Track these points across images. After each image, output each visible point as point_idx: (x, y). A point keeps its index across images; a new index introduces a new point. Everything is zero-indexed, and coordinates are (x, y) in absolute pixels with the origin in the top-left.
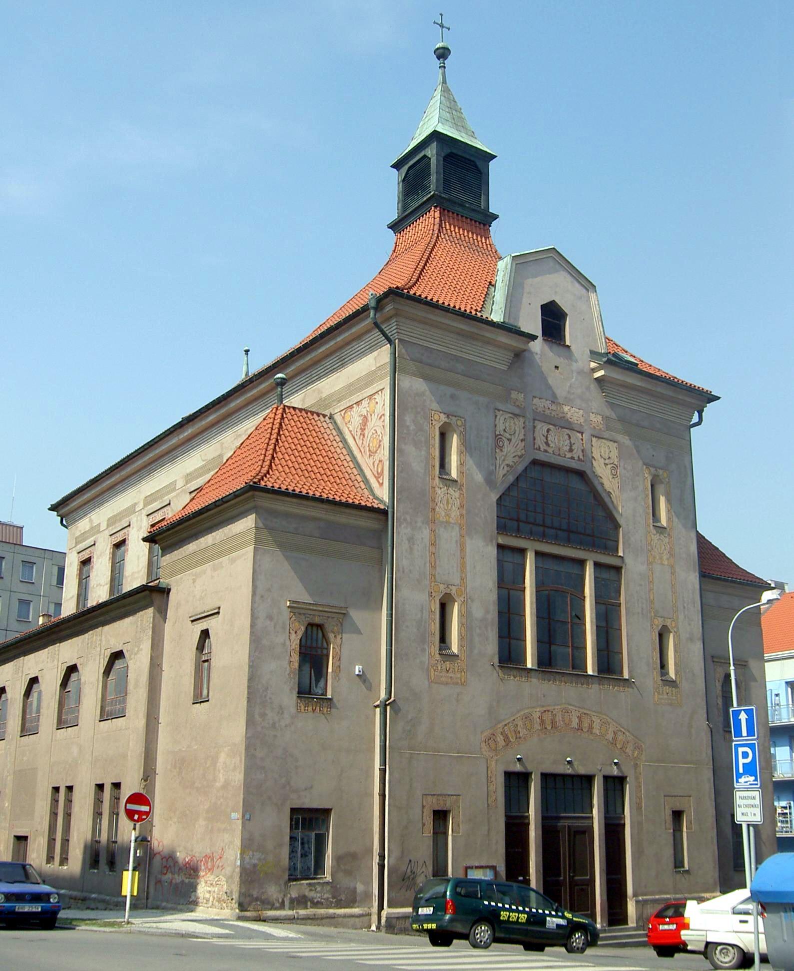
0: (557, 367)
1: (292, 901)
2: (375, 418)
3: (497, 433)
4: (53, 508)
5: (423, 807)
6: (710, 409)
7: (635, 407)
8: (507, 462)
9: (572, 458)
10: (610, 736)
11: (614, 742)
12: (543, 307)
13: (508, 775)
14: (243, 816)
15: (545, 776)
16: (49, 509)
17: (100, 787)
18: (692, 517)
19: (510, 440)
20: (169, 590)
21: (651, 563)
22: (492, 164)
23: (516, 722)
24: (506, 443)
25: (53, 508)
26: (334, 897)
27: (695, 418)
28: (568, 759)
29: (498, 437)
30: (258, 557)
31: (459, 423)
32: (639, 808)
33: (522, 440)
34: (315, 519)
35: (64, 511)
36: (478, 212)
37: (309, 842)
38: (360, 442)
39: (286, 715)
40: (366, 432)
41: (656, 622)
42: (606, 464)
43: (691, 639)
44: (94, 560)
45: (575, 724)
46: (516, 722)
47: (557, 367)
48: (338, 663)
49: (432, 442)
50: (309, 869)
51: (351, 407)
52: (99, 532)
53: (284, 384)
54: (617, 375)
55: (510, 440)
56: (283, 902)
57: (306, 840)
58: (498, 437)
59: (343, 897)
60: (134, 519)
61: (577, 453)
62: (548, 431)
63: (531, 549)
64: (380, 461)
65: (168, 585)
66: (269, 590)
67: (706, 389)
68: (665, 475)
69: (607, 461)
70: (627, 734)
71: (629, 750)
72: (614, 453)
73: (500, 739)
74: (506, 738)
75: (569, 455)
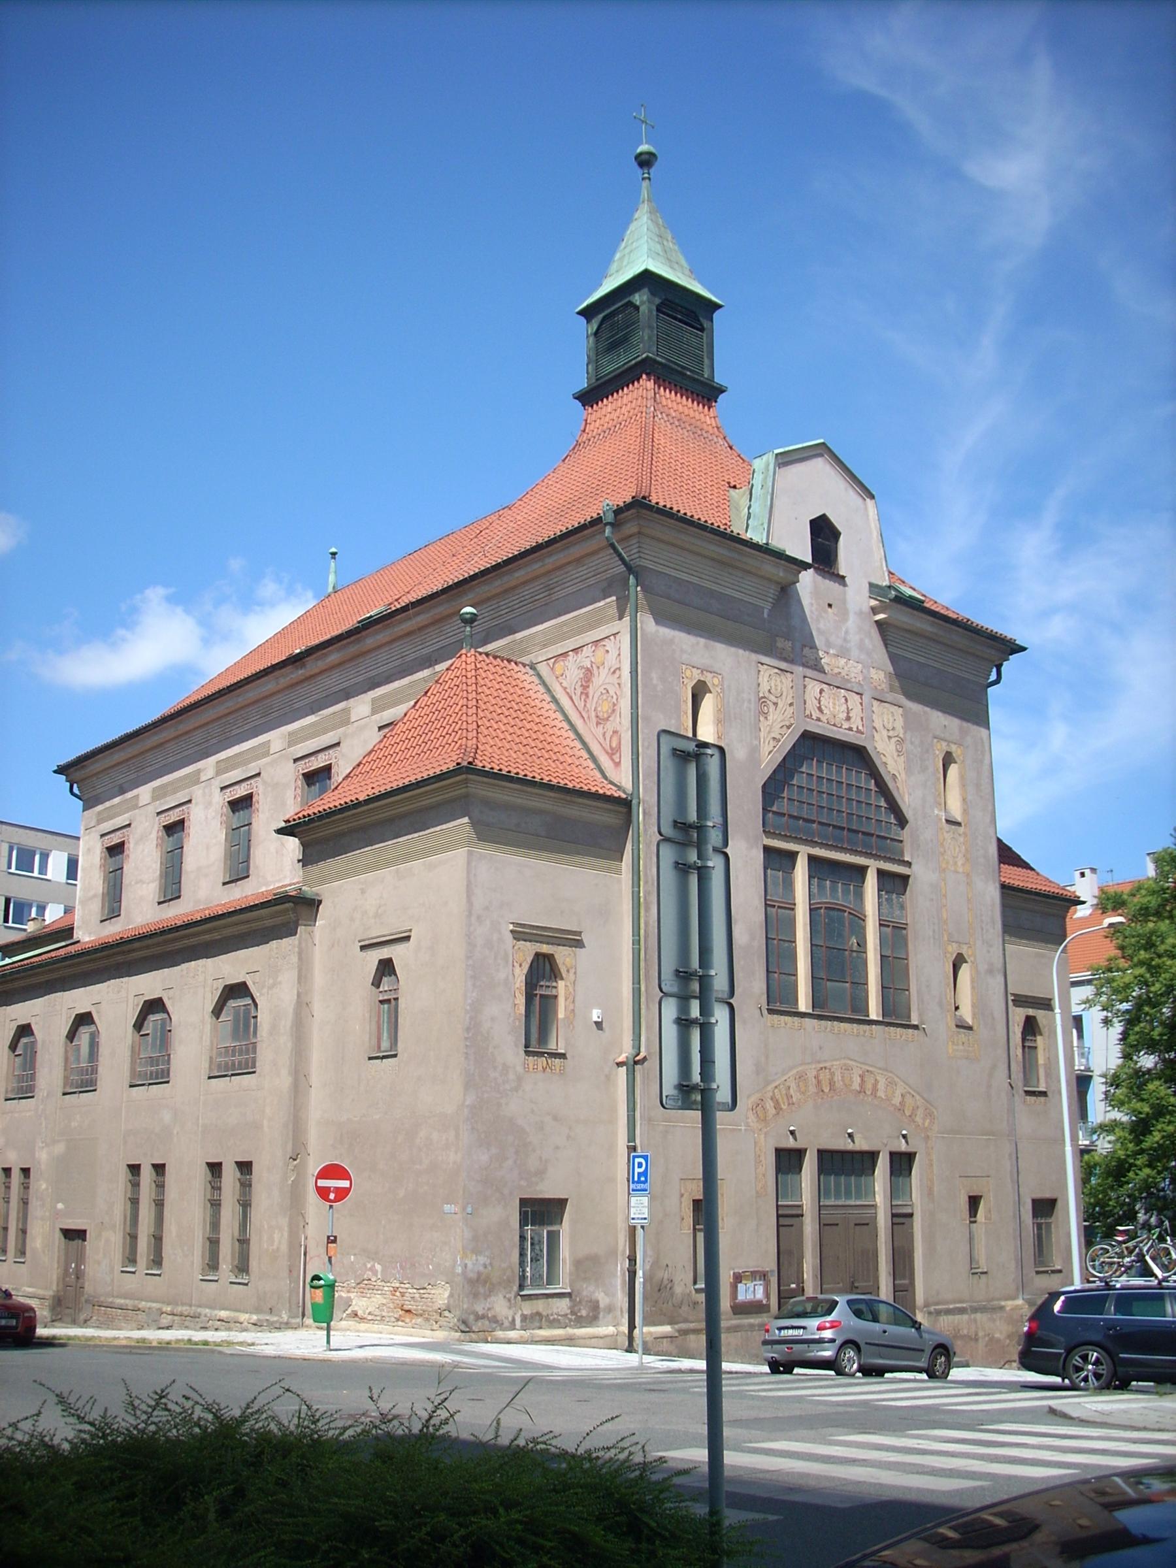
0: (830, 606)
1: (524, 1318)
2: (604, 672)
3: (761, 695)
4: (61, 770)
5: (682, 1195)
6: (1010, 666)
7: (922, 660)
8: (773, 735)
9: (850, 729)
10: (897, 1100)
11: (901, 1109)
12: (812, 522)
13: (779, 1152)
14: (464, 1209)
15: (821, 1153)
16: (55, 772)
17: (215, 1168)
18: (990, 808)
19: (776, 704)
20: (320, 902)
21: (944, 870)
22: (717, 315)
23: (787, 1084)
24: (772, 707)
25: (61, 770)
26: (573, 1313)
27: (993, 677)
28: (850, 1131)
29: (762, 701)
30: (473, 864)
31: (716, 681)
32: (930, 1193)
33: (791, 704)
34: (540, 812)
35: (78, 775)
36: (702, 383)
37: (540, 1242)
38: (581, 705)
39: (511, 1076)
40: (591, 691)
41: (950, 949)
42: (889, 737)
43: (990, 971)
44: (130, 847)
45: (856, 1086)
46: (787, 1084)
47: (830, 606)
48: (571, 1007)
49: (683, 707)
50: (541, 1276)
52: (136, 807)
54: (905, 618)
55: (776, 704)
56: (514, 1320)
57: (536, 1239)
58: (762, 701)
59: (584, 1313)
60: (197, 792)
61: (856, 723)
62: (821, 691)
63: (803, 852)
64: (615, 732)
65: (317, 894)
66: (487, 908)
67: (1009, 636)
68: (959, 752)
69: (891, 733)
70: (918, 1097)
71: (918, 1119)
72: (899, 723)
73: (769, 1105)
74: (777, 1106)
75: (846, 725)
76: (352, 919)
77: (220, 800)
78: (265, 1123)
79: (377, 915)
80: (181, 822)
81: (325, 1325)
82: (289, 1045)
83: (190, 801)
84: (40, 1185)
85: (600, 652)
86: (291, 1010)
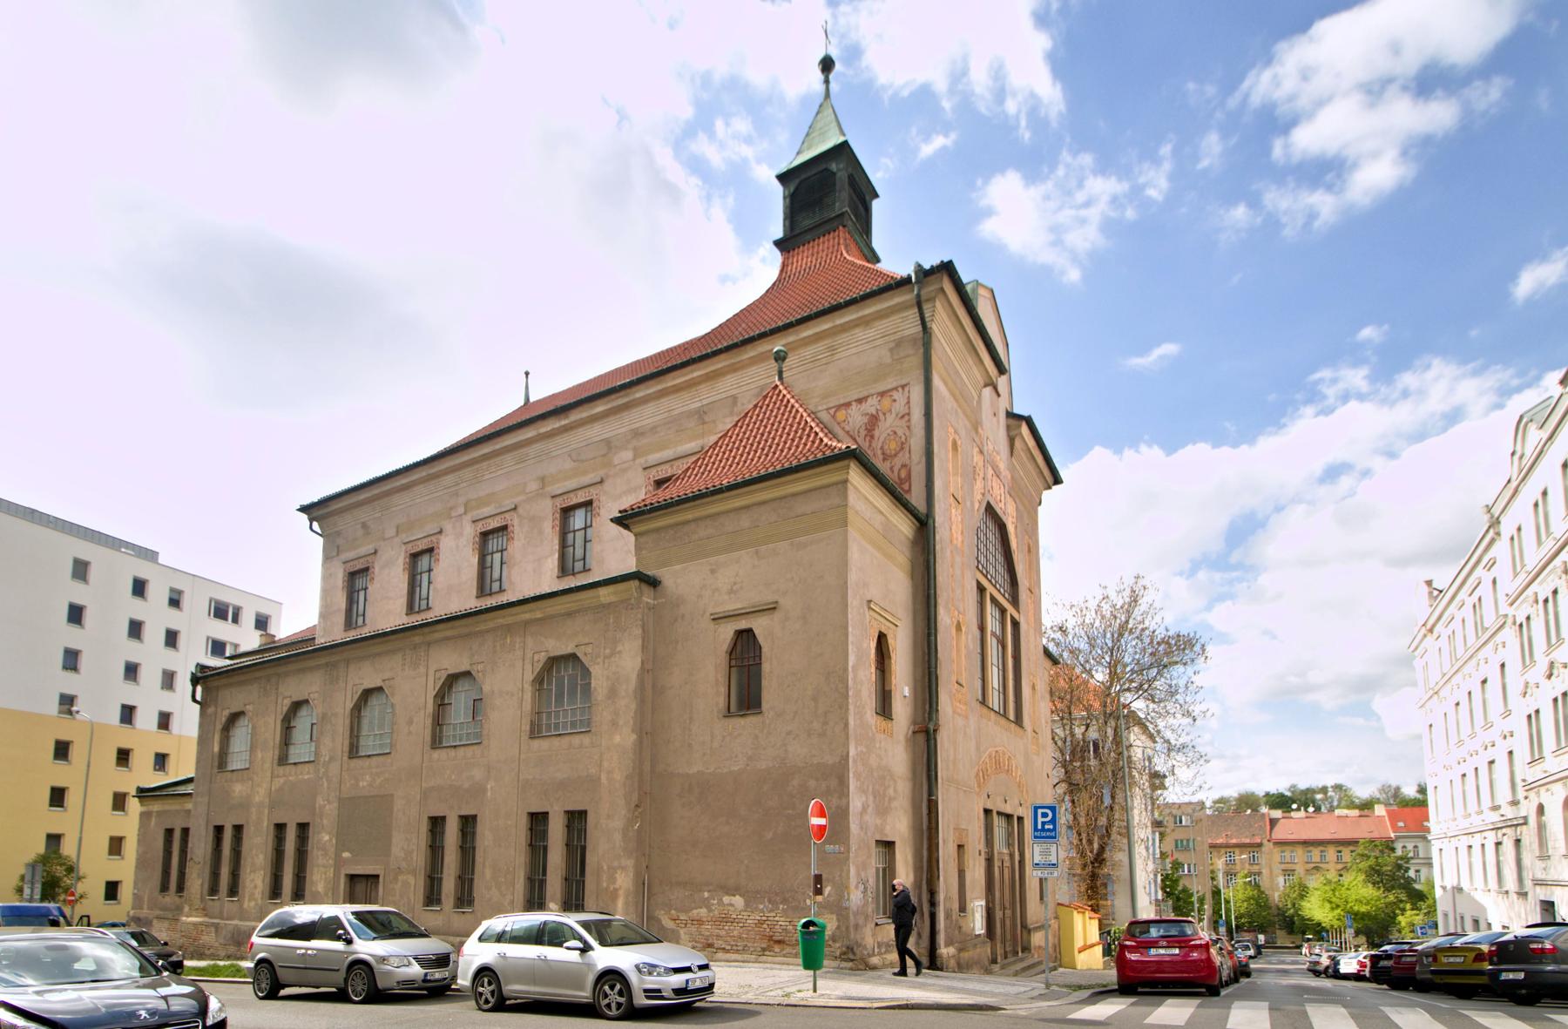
2: (890, 419)
4: (303, 509)
25: (303, 509)
40: (876, 433)
51: (848, 405)
53: (784, 359)
64: (904, 466)
76: (700, 596)
77: (470, 532)
78: (603, 777)
79: (731, 591)
80: (367, 569)
81: (1367, 973)
82: (633, 706)
83: (440, 532)
84: (323, 838)
85: (886, 401)
86: (634, 677)
